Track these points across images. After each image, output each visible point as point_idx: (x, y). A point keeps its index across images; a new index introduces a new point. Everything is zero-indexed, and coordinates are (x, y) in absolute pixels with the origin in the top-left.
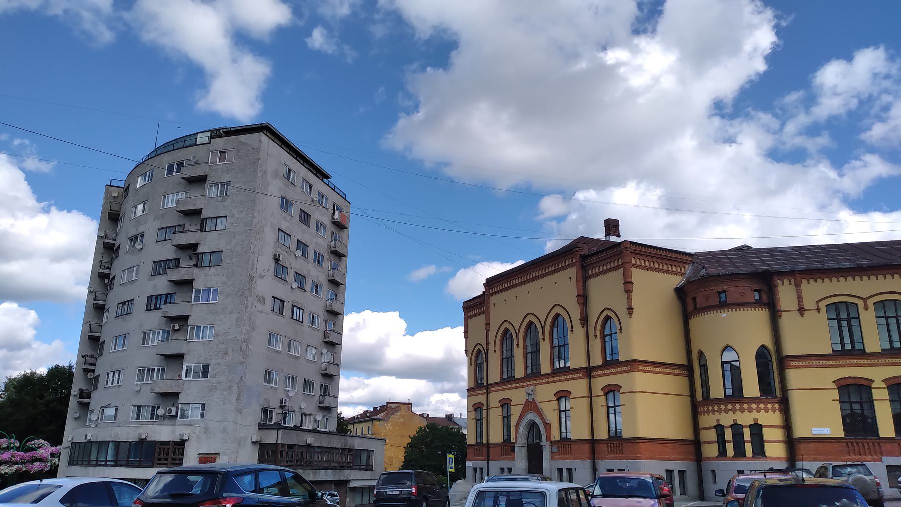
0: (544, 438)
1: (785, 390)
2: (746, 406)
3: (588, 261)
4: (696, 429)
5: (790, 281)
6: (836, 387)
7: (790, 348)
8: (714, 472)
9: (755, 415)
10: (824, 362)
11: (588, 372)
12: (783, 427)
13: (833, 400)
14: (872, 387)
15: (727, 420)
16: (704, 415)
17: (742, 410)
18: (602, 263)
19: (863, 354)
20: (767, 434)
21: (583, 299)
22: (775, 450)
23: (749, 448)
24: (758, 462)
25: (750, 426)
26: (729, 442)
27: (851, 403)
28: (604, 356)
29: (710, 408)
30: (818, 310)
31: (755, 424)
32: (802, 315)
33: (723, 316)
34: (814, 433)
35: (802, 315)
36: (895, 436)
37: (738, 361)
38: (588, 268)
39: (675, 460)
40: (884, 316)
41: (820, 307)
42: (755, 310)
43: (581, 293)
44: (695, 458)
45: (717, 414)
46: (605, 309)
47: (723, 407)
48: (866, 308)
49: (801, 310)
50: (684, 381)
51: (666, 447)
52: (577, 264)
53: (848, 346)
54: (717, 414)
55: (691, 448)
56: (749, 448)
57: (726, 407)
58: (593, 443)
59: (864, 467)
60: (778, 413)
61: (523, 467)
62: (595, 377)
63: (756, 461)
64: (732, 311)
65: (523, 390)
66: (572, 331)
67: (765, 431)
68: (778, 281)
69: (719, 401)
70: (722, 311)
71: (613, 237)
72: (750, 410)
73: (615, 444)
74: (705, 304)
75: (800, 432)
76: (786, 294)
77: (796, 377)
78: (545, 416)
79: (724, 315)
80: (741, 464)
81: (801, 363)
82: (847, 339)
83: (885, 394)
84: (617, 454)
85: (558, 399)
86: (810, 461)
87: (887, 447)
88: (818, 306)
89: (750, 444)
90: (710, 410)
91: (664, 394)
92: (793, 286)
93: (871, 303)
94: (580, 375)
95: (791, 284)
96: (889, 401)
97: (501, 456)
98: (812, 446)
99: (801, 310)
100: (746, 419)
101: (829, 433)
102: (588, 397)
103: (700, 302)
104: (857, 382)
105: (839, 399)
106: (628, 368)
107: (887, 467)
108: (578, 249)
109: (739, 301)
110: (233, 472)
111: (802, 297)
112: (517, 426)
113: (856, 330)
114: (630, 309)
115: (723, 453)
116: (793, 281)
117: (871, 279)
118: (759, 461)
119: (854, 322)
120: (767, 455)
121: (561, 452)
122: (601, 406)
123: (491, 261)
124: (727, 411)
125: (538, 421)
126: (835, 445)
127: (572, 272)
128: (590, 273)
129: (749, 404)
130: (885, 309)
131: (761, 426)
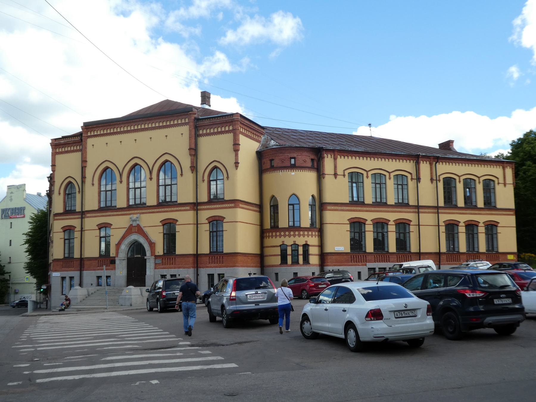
0: (148, 253)
2: (282, 233)
3: (201, 123)
4: (262, 247)
5: (331, 156)
6: (349, 223)
7: (328, 198)
8: (277, 274)
9: (306, 238)
10: (344, 208)
11: (196, 206)
12: (319, 246)
14: (411, 224)
15: (289, 241)
17: (299, 235)
18: (214, 126)
19: (385, 205)
21: (194, 151)
22: (314, 260)
23: (289, 259)
24: (305, 267)
25: (291, 245)
27: (355, 233)
28: (209, 195)
29: (274, 234)
30: (344, 175)
31: (306, 244)
32: (336, 178)
33: (292, 174)
34: (336, 249)
35: (336, 178)
36: (373, 252)
37: (146, 198)
38: (199, 128)
39: (252, 267)
41: (345, 174)
42: (303, 171)
43: (193, 146)
44: (260, 265)
45: (292, 237)
47: (287, 233)
48: (367, 177)
50: (257, 214)
52: (192, 124)
53: (378, 200)
54: (282, 237)
55: (258, 259)
56: (301, 258)
57: (290, 233)
58: (439, 254)
59: (431, 268)
60: (317, 237)
61: (124, 275)
62: (201, 210)
63: (305, 266)
64: (298, 171)
65: (128, 217)
66: (182, 175)
68: (325, 155)
69: (284, 229)
70: (292, 170)
71: (207, 105)
72: (280, 236)
73: (216, 257)
74: (280, 165)
75: (328, 249)
76: (328, 162)
77: (330, 216)
78: (150, 237)
79: (293, 174)
80: (295, 269)
84: (217, 263)
86: (333, 266)
87: (369, 257)
88: (344, 173)
89: (302, 256)
91: (249, 224)
92: (332, 159)
93: (370, 173)
94: (188, 208)
95: (331, 157)
96: (373, 232)
97: (98, 266)
98: (334, 257)
99: (505, 184)
100: (301, 241)
101: (343, 250)
103: (275, 163)
104: (359, 220)
105: (349, 230)
106: (232, 205)
107: (368, 268)
108: (193, 112)
109: (303, 165)
111: (337, 167)
112: (118, 245)
113: (361, 190)
114: (237, 164)
116: (333, 156)
117: (407, 162)
118: (306, 266)
119: (405, 187)
120: (310, 263)
121: (165, 263)
122: (205, 231)
124: (290, 236)
125: (142, 240)
126: (345, 257)
127: (185, 130)
128: (201, 132)
129: (303, 231)
131: (308, 245)
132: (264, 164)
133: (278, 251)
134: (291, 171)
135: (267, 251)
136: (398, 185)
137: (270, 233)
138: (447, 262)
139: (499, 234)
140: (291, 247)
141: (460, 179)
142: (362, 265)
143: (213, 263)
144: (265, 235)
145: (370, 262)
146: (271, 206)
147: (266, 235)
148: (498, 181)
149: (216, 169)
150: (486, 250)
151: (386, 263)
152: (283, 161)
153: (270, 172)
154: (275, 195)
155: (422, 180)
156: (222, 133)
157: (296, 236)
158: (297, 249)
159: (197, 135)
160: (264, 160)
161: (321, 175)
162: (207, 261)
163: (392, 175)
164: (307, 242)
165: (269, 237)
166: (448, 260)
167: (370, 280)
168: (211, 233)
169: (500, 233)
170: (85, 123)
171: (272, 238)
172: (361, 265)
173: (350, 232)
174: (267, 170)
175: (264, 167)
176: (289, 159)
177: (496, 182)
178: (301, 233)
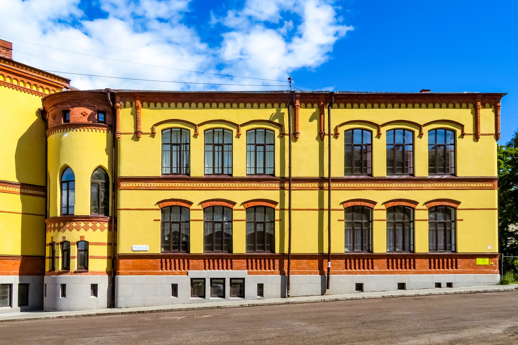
1: (116, 209)
8: (64, 286)
9: (82, 232)
13: (339, 220)
16: (50, 232)
19: (231, 179)
20: (92, 251)
24: (80, 276)
30: (153, 134)
40: (254, 143)
48: (379, 135)
49: (137, 135)
67: (91, 248)
81: (131, 184)
82: (260, 164)
83: (383, 215)
99: (476, 136)
102: (120, 209)
115: (66, 268)
123: (296, 70)
129: (85, 222)
131: (87, 243)
136: (256, 145)
137: (56, 224)
138: (346, 270)
139: (458, 223)
145: (195, 268)
146: (62, 183)
148: (463, 131)
154: (69, 165)
155: (301, 137)
163: (243, 130)
166: (432, 265)
169: (462, 220)
172: (178, 273)
173: (247, 222)
177: (459, 132)
178: (74, 224)
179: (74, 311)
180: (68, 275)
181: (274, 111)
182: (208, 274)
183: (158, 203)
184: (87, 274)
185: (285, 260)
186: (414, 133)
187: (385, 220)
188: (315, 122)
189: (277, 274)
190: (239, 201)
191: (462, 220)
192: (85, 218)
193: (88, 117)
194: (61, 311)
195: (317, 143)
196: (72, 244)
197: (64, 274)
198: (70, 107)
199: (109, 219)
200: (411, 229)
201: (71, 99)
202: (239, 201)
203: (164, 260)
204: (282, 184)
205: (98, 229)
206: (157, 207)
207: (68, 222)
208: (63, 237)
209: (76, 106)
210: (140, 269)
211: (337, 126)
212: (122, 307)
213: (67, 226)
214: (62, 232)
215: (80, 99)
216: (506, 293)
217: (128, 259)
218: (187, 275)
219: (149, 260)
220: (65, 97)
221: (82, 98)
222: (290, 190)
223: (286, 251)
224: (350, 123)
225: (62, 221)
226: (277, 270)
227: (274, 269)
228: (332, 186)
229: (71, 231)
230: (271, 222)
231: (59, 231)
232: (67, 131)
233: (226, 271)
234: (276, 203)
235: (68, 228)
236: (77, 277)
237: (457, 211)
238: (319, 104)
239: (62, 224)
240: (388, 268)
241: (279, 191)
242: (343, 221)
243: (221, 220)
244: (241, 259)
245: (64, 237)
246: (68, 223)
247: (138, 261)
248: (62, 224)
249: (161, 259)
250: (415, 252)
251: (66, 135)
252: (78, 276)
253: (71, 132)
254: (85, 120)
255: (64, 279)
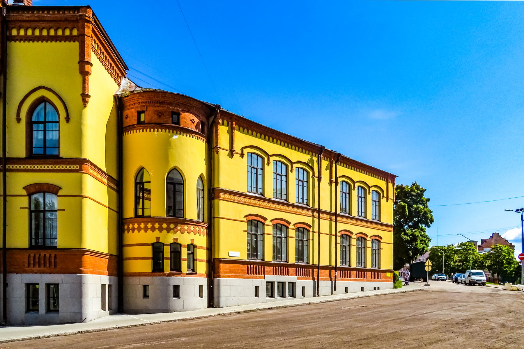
8: (177, 288)
9: (192, 236)
19: (262, 198)
24: (191, 277)
26: (167, 259)
30: (242, 155)
45: (157, 231)
46: (40, 88)
51: (102, 261)
54: (157, 231)
63: (190, 276)
72: (153, 229)
85: (30, 195)
90: (131, 228)
107: (267, 282)
110: (60, 341)
114: (85, 97)
116: (230, 123)
122: (21, 208)
124: (168, 230)
128: (14, 32)
130: (36, 147)
131: (195, 247)
132: (127, 118)
133: (148, 252)
134: (173, 133)
135: (131, 252)
136: (299, 181)
140: (170, 247)
141: (269, 160)
142: (260, 278)
143: (37, 265)
144: (126, 227)
147: (128, 228)
149: (43, 105)
150: (296, 259)
151: (285, 276)
152: (160, 114)
153: (138, 131)
156: (56, 39)
157: (149, 230)
158: (491, 281)
159: (7, 36)
160: (127, 112)
161: (214, 148)
162: (24, 262)
164: (194, 242)
165: (133, 230)
167: (472, 285)
168: (33, 214)
169: (244, 231)
170: (401, 287)
171: (133, 232)
174: (131, 128)
175: (127, 122)
176: (171, 114)
178: (186, 227)
179: (188, 311)
180: (182, 276)
181: (309, 157)
182: (277, 278)
183: (246, 216)
184: (197, 276)
185: (314, 269)
186: (380, 195)
187: (294, 238)
188: (328, 171)
189: (310, 280)
190: (355, 232)
191: (244, 231)
192: (160, 220)
193: (196, 126)
194: (175, 312)
195: (329, 187)
196: (184, 246)
197: (177, 275)
198: (181, 110)
199: (207, 225)
200: (34, 218)
201: (181, 103)
202: (355, 232)
203: (249, 266)
204: (313, 213)
205: (149, 230)
206: (245, 219)
207: (179, 224)
208: (174, 238)
209: (187, 112)
210: (234, 273)
211: (242, 148)
212: (223, 306)
213: (179, 228)
214: (172, 234)
215: (189, 105)
216: (420, 292)
217: (226, 263)
218: (264, 279)
219: (240, 265)
220: (177, 99)
221: (191, 105)
222: (319, 218)
223: (316, 263)
224: (277, 155)
225: (173, 223)
226: (311, 277)
227: (309, 276)
228: (221, 196)
229: (183, 234)
230: (261, 234)
231: (168, 232)
232: (177, 133)
233: (276, 276)
234: (310, 226)
235: (179, 230)
236: (190, 278)
237: (265, 226)
238: (330, 160)
239: (172, 226)
240: (371, 278)
241: (311, 218)
242: (246, 232)
243: (281, 236)
244: (293, 267)
245: (192, 240)
246: (179, 225)
247: (233, 266)
248: (172, 226)
249: (248, 265)
250: (264, 260)
251: (175, 137)
252: (190, 278)
253: (181, 135)
254: (193, 128)
255: (176, 280)
